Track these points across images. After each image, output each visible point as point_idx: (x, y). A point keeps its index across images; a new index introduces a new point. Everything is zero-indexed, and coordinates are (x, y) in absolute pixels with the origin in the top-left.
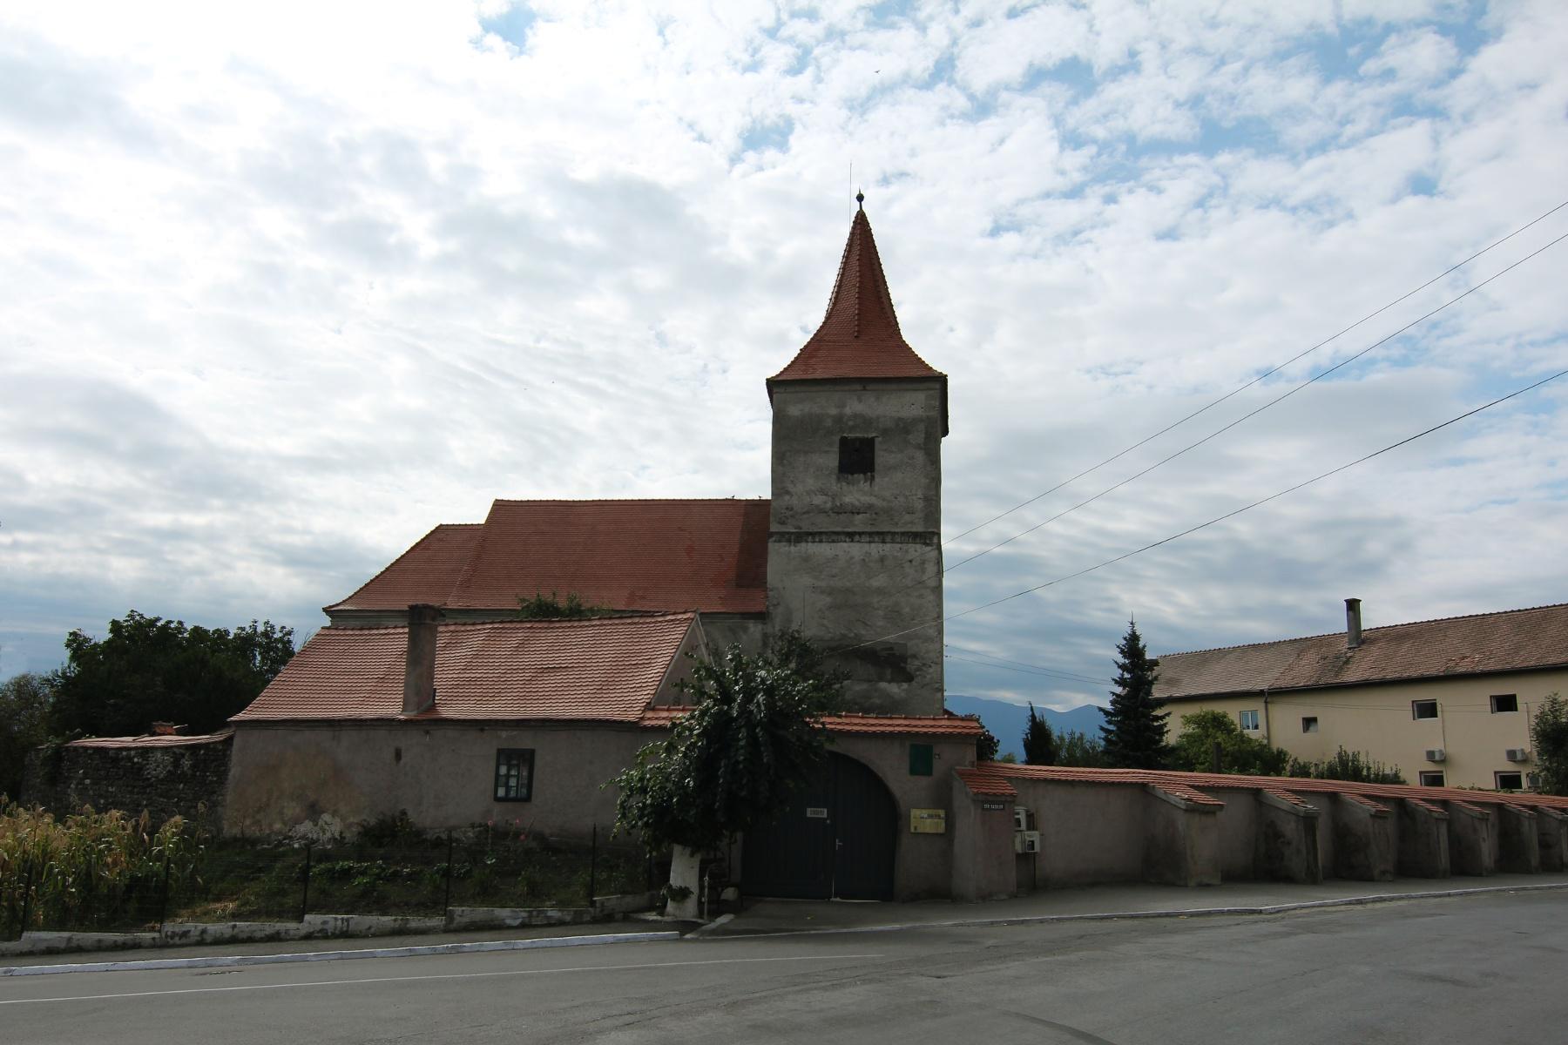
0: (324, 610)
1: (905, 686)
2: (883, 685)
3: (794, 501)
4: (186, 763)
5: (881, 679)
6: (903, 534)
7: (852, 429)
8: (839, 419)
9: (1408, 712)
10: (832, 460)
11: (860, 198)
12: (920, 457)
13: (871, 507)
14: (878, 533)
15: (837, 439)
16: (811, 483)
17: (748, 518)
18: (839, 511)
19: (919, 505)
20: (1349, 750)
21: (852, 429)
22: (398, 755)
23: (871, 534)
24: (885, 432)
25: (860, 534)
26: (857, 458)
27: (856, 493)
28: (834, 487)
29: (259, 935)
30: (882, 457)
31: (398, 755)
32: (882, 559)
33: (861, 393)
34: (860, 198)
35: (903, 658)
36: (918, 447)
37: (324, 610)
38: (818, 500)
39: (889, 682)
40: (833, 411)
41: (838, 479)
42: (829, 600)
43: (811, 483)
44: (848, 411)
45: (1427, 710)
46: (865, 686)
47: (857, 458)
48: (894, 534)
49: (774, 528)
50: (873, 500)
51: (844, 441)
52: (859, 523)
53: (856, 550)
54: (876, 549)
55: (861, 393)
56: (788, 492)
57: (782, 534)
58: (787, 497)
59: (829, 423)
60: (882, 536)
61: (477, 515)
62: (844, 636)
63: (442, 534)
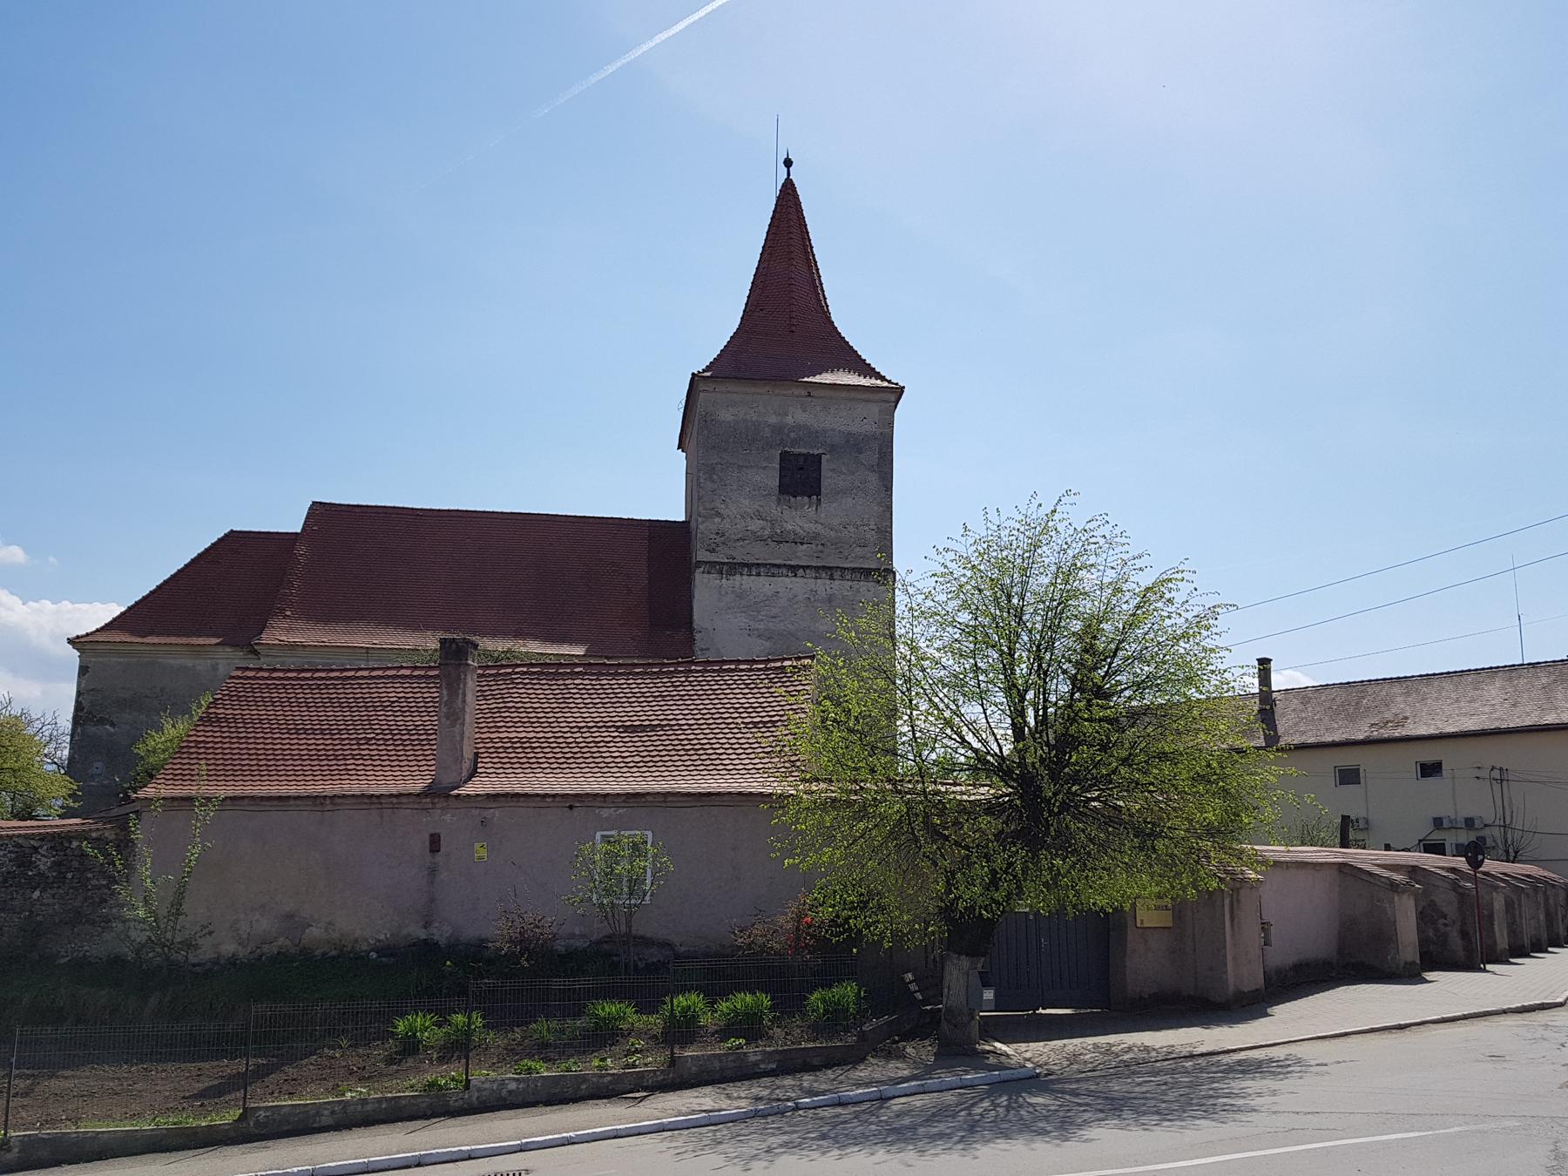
0: (70, 641)
3: (726, 525)
4: (44, 863)
6: (853, 569)
7: (795, 442)
8: (778, 430)
9: (1413, 771)
10: (770, 478)
11: (788, 163)
12: (873, 478)
13: (817, 536)
14: (824, 568)
16: (746, 504)
17: (663, 548)
18: (781, 539)
19: (871, 536)
21: (795, 442)
22: (435, 843)
23: (817, 568)
24: (833, 449)
25: (805, 568)
26: (800, 477)
27: (799, 518)
28: (774, 510)
30: (830, 478)
31: (435, 843)
32: (830, 599)
33: (789, 382)
34: (788, 163)
36: (871, 469)
37: (70, 641)
38: (755, 525)
40: (773, 420)
42: (768, 644)
43: (746, 504)
44: (789, 420)
45: (1349, 776)
47: (800, 477)
49: (702, 555)
51: (785, 456)
52: (802, 555)
53: (798, 586)
54: (823, 586)
55: (789, 382)
56: (718, 514)
57: (713, 564)
58: (717, 520)
59: (767, 432)
61: (286, 517)
63: (234, 542)
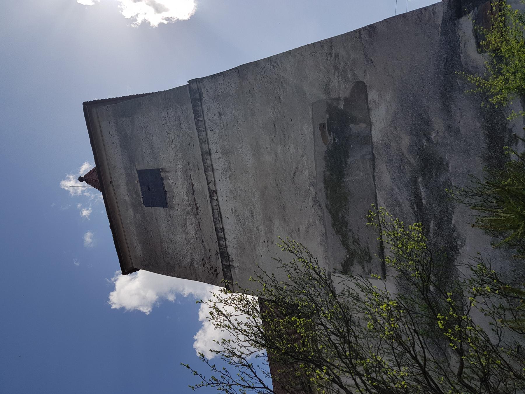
1: (373, 95)
2: (376, 136)
3: (196, 256)
5: (367, 140)
10: (160, 212)
13: (185, 171)
15: (147, 209)
20: (124, 305)
27: (177, 185)
29: (356, 174)
32: (226, 153)
35: (331, 109)
39: (370, 124)
41: (172, 208)
42: (277, 222)
46: (382, 167)
48: (201, 142)
50: (179, 168)
54: (218, 162)
60: (208, 169)
62: (315, 201)
